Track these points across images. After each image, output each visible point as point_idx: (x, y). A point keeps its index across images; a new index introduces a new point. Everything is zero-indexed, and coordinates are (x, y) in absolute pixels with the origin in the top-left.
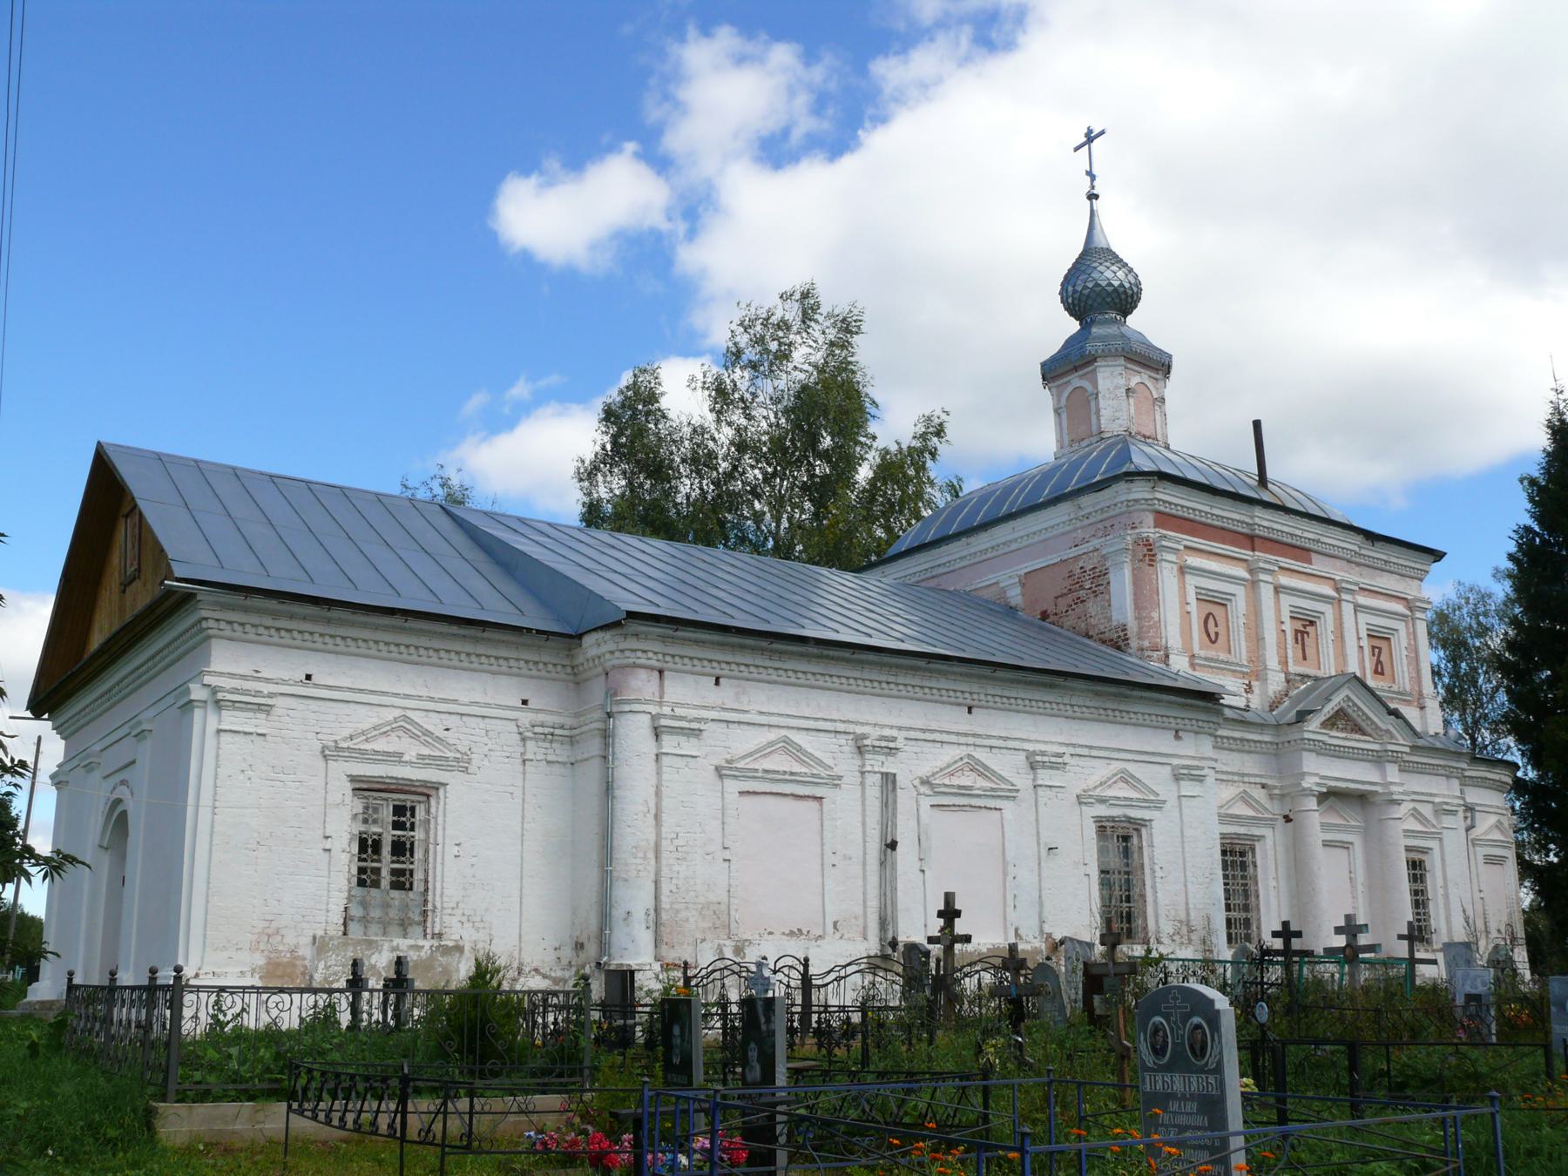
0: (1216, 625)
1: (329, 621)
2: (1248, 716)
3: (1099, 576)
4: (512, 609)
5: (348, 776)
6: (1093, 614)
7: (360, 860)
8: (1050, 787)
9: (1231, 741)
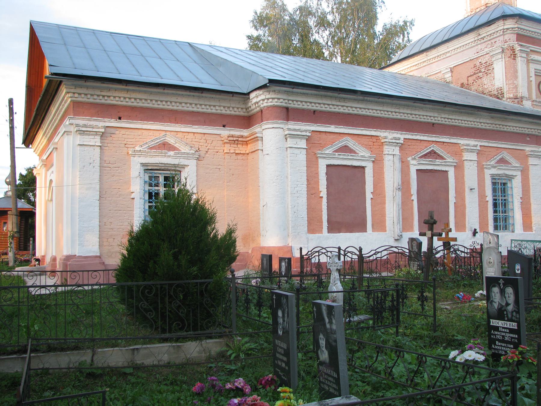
1: (128, 91)
3: (489, 66)
4: (216, 83)
5: (141, 164)
7: (149, 202)
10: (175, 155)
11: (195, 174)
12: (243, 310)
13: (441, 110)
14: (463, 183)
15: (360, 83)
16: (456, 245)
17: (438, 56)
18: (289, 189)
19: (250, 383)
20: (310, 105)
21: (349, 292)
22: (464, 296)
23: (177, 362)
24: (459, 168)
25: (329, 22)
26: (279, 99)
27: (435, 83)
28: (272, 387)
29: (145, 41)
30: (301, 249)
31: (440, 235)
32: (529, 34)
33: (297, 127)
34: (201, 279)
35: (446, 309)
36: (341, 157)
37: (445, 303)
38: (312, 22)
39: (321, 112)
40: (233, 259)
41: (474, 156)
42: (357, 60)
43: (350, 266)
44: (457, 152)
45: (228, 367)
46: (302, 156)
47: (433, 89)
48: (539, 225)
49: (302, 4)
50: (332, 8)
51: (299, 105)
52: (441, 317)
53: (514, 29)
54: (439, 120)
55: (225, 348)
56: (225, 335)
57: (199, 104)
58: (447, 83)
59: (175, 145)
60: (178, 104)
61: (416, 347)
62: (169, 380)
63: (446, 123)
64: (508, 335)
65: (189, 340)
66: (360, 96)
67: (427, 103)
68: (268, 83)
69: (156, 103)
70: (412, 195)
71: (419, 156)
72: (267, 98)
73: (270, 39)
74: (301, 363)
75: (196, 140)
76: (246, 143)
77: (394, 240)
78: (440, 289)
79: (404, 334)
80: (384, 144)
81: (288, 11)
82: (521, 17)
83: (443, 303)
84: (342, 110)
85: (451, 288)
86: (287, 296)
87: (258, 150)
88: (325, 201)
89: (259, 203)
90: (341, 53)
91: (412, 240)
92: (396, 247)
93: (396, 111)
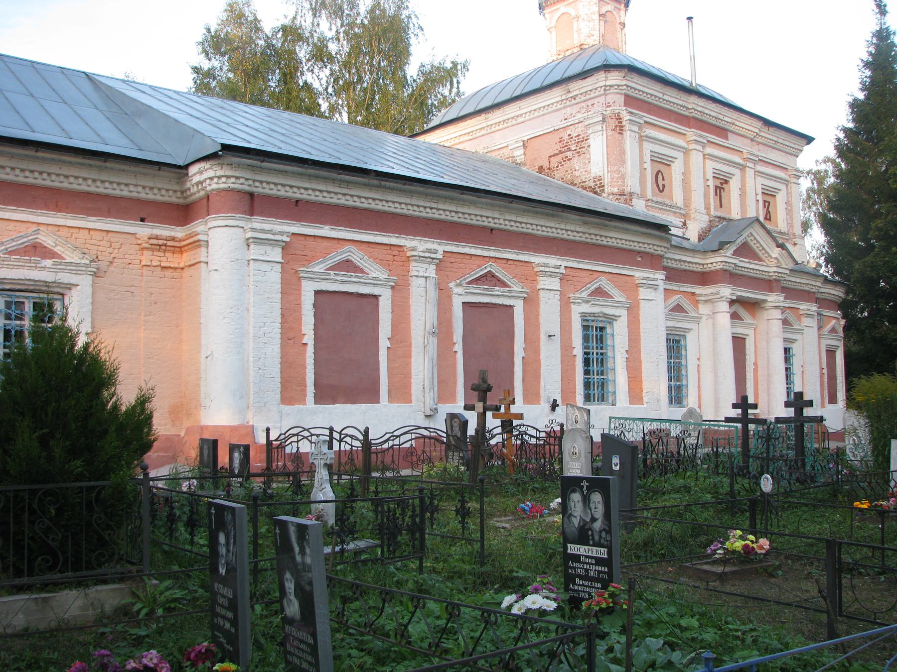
0: (663, 180)
1: (37, 159)
2: (685, 244)
3: (582, 141)
4: (131, 145)
6: (577, 168)
7: (5, 347)
8: (550, 290)
9: (673, 262)
10: (54, 267)
11: (90, 300)
12: (164, 534)
13: (505, 207)
14: (537, 326)
15: (377, 158)
16: (524, 425)
17: (504, 121)
18: (251, 330)
19: (170, 658)
20: (291, 190)
21: (343, 502)
22: (533, 507)
23: (42, 626)
24: (531, 301)
25: (330, 54)
26: (237, 178)
27: (496, 163)
28: (206, 664)
29: (5, 62)
30: (268, 430)
31: (497, 408)
32: (642, 97)
33: (278, 228)
34: (89, 481)
35: (503, 528)
36: (339, 278)
37: (503, 518)
38: (303, 52)
39: (308, 202)
40: (147, 446)
41: (555, 284)
42: (374, 120)
43: (349, 459)
44: (529, 276)
45: (133, 631)
46: (275, 275)
47: (494, 174)
48: (653, 395)
49: (287, 22)
50: (337, 31)
51: (271, 189)
52: (494, 542)
53: (620, 88)
54: (501, 224)
55: (128, 600)
56: (131, 578)
57: (99, 180)
58: (516, 164)
59: (55, 250)
60: (62, 178)
61: (452, 590)
62: (23, 660)
63: (512, 229)
64: (594, 568)
65: (65, 588)
66: (373, 179)
67: (482, 195)
68: (220, 151)
69: (22, 174)
70: (455, 343)
71: (467, 281)
72: (218, 175)
73: (231, 75)
74: (259, 621)
75: (93, 242)
76: (180, 250)
77: (423, 417)
78: (496, 496)
79: (434, 570)
80: (411, 259)
81: (263, 31)
82: (632, 69)
83: (498, 519)
84: (342, 201)
85: (513, 495)
86: (233, 509)
87: (200, 262)
88: (310, 350)
89: (200, 352)
90: (349, 107)
91: (452, 417)
92: (425, 428)
93: (432, 206)
